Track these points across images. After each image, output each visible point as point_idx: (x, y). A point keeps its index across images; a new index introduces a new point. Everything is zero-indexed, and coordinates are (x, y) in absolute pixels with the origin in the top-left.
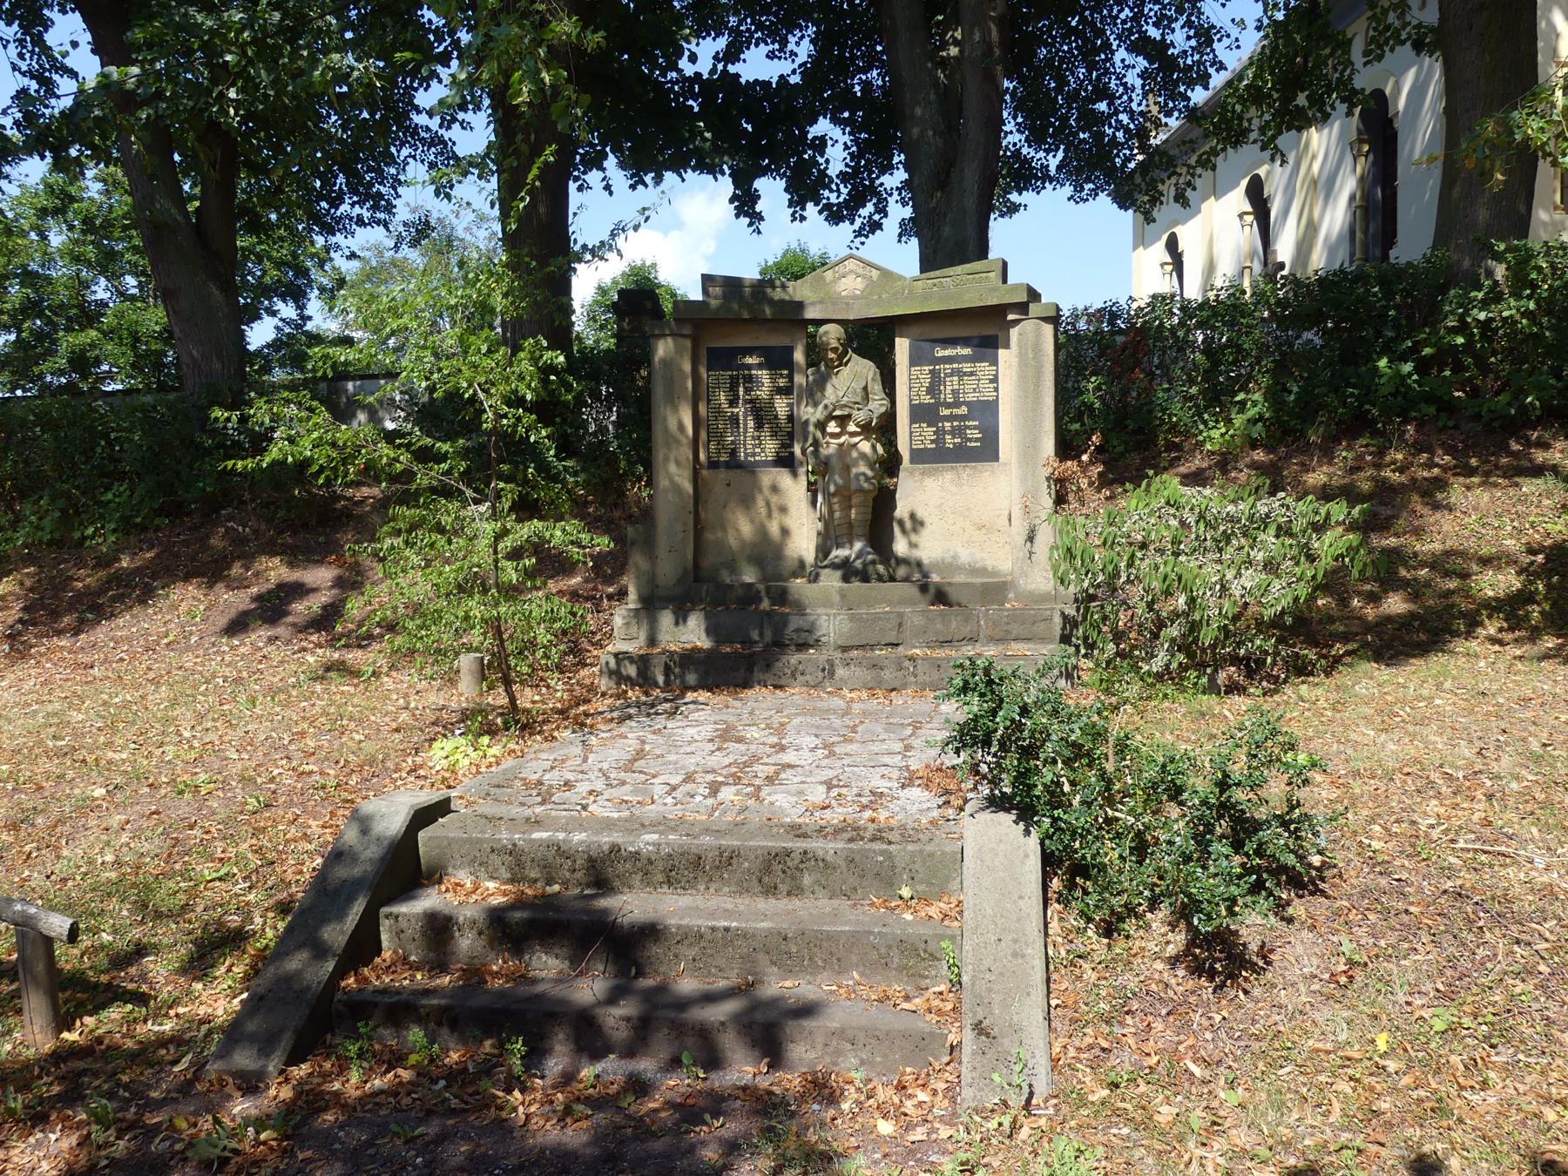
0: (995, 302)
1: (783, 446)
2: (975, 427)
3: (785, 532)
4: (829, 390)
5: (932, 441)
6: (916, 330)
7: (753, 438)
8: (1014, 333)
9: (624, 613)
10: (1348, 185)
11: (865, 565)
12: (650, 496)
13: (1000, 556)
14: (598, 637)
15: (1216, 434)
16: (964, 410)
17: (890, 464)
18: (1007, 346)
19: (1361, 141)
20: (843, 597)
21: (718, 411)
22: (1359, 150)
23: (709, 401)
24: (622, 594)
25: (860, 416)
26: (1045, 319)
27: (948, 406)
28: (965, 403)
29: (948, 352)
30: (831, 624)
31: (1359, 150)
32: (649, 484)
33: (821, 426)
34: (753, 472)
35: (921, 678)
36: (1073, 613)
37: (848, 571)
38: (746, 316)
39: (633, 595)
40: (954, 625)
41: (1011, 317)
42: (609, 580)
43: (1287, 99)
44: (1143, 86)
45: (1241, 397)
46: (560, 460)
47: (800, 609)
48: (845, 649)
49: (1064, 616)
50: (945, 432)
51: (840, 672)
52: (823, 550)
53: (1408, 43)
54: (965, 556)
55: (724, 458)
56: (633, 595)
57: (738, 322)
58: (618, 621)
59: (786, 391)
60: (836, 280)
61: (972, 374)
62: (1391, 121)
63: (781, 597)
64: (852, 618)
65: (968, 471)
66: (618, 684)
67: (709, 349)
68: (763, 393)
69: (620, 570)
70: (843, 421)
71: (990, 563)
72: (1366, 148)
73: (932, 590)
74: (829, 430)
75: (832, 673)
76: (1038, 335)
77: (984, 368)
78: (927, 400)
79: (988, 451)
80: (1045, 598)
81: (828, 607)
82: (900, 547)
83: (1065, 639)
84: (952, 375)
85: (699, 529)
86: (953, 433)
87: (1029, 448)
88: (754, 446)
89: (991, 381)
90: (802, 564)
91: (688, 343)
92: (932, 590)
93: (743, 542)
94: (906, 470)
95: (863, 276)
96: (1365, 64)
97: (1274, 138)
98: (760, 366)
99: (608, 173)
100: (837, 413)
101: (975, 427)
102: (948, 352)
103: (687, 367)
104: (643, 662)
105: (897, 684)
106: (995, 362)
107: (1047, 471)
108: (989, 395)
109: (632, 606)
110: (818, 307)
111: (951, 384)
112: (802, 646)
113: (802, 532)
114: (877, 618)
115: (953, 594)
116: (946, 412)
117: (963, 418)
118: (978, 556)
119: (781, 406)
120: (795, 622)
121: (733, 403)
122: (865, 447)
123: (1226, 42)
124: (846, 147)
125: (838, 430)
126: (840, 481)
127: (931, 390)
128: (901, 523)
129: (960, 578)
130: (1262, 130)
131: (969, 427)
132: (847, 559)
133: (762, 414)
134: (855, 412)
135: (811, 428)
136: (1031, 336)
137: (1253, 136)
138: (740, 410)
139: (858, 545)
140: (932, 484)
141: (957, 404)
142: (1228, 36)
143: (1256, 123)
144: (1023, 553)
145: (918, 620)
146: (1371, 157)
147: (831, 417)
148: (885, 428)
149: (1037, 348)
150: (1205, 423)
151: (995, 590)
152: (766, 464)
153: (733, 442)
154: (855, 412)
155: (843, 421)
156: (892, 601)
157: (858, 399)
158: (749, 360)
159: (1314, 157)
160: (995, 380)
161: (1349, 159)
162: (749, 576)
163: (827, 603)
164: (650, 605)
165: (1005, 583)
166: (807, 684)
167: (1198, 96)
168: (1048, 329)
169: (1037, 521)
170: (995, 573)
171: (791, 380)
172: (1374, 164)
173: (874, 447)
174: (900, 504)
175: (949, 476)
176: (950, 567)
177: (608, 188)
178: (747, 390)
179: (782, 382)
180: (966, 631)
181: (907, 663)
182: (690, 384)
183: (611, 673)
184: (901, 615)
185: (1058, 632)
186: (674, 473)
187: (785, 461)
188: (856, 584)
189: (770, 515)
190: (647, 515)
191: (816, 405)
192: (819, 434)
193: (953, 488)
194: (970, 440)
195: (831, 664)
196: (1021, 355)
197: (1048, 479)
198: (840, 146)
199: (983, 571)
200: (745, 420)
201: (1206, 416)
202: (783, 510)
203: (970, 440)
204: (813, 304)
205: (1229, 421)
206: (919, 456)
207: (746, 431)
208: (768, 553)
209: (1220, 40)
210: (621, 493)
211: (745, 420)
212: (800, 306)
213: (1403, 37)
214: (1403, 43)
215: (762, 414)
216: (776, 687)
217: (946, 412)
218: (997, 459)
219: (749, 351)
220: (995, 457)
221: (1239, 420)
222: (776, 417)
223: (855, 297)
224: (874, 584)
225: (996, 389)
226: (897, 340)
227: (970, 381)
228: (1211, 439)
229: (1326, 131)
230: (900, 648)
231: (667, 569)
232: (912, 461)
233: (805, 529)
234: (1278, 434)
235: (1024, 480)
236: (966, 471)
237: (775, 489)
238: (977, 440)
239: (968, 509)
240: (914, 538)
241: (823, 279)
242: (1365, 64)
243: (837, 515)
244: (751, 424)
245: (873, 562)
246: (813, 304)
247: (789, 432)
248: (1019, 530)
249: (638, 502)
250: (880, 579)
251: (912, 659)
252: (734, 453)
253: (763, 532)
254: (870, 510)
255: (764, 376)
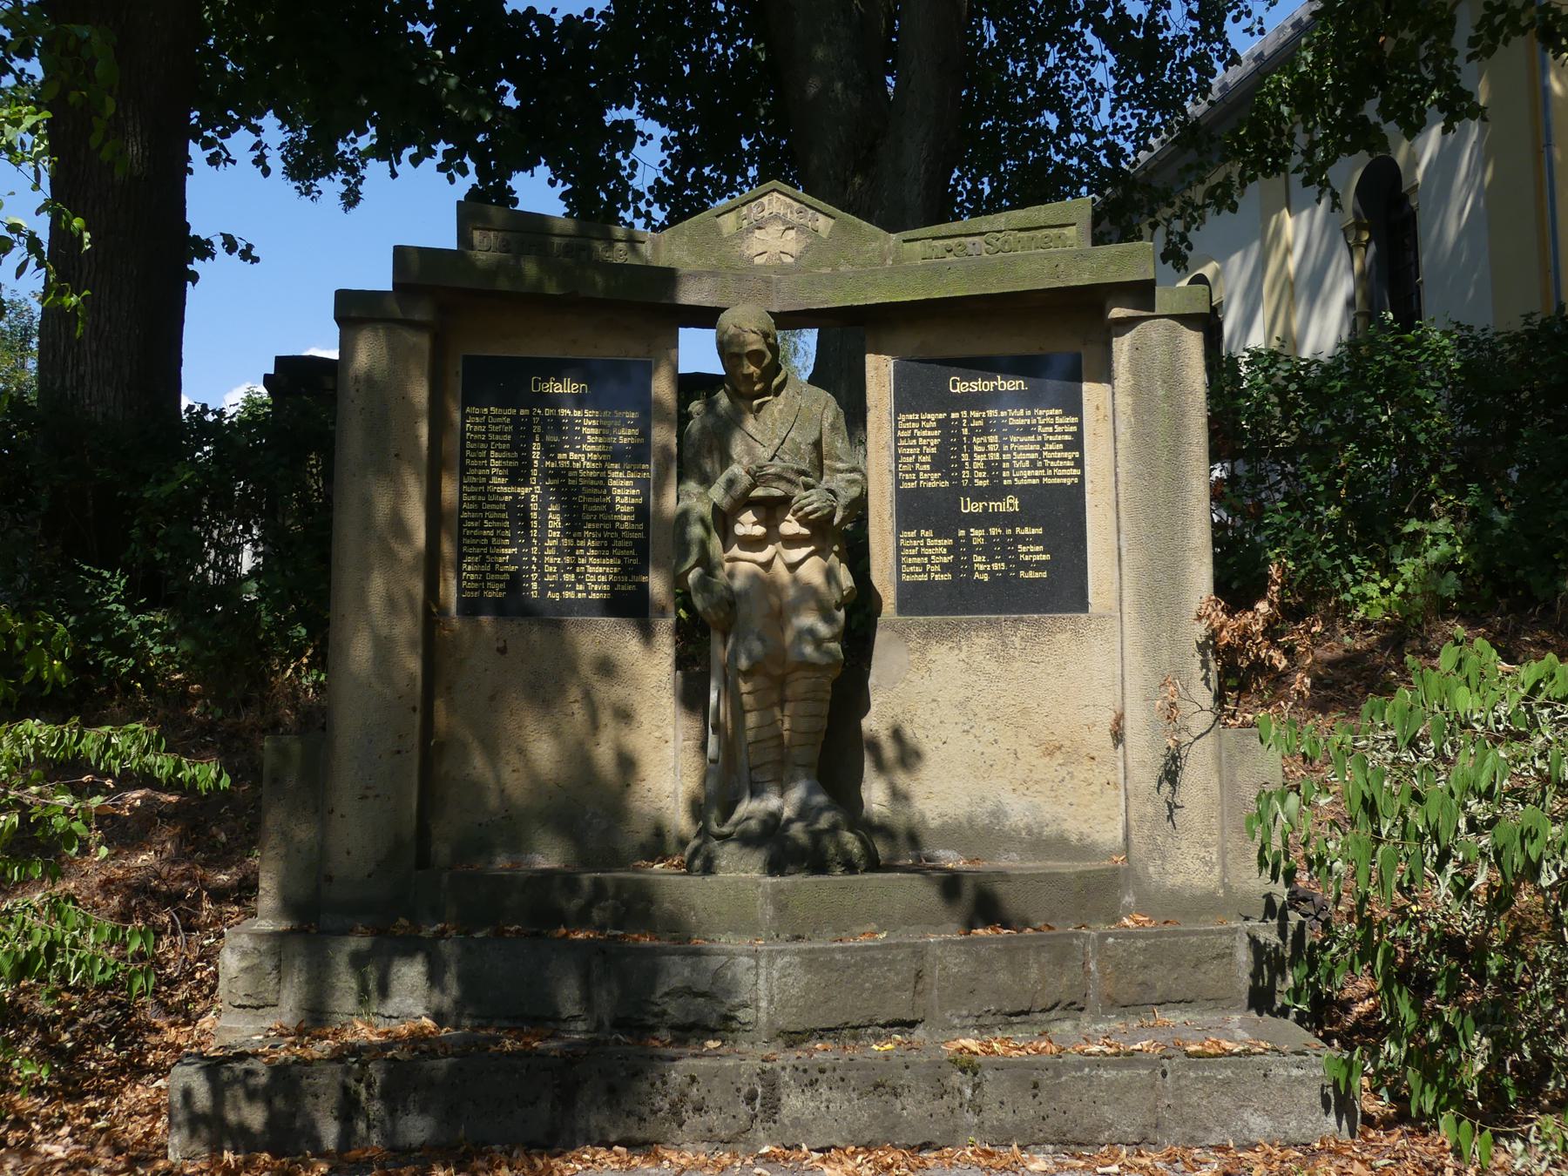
0: (1085, 279)
1: (625, 570)
2: (1036, 540)
3: (627, 764)
4: (737, 448)
5: (945, 568)
6: (911, 341)
7: (560, 551)
8: (1122, 347)
9: (246, 941)
10: (1342, 288)
11: (816, 836)
12: (317, 685)
13: (1094, 811)
14: (180, 996)
15: (1372, 590)
16: (1011, 504)
17: (859, 617)
18: (1105, 374)
19: (1358, 226)
20: (781, 907)
21: (484, 491)
22: (1357, 238)
23: (464, 470)
24: (245, 891)
25: (812, 500)
26: (1187, 320)
27: (979, 494)
28: (1012, 489)
29: (978, 386)
30: (765, 977)
31: (1357, 238)
32: (320, 661)
33: (723, 520)
34: (558, 625)
35: (993, 1115)
36: (1274, 939)
37: (780, 849)
38: (552, 288)
39: (267, 899)
40: (1034, 973)
41: (1117, 313)
42: (221, 859)
43: (1353, 106)
44: (1117, 89)
45: (1413, 525)
46: (134, 611)
47: (680, 933)
48: (793, 1038)
49: (1256, 945)
50: (971, 550)
51: (794, 1103)
52: (714, 801)
53: (1532, 32)
54: (1019, 811)
55: (494, 592)
56: (267, 899)
57: (533, 303)
58: (230, 962)
59: (637, 455)
60: (743, 233)
61: (1027, 430)
62: (1404, 198)
63: (638, 906)
64: (812, 961)
65: (1024, 631)
66: (216, 1150)
67: (468, 360)
68: (583, 457)
69: (249, 837)
70: (771, 510)
71: (1073, 827)
72: (1366, 236)
73: (968, 891)
74: (740, 530)
75: (772, 1107)
76: (1175, 351)
77: (1051, 418)
78: (934, 481)
79: (1064, 590)
80: (1206, 904)
81: (752, 936)
82: (875, 795)
83: (1261, 1000)
84: (985, 431)
85: (433, 752)
86: (988, 550)
87: (1160, 590)
88: (562, 569)
89: (1068, 446)
90: (659, 832)
91: (423, 342)
92: (968, 891)
93: (534, 777)
94: (891, 626)
95: (801, 229)
96: (1469, 58)
97: (1324, 166)
98: (579, 401)
99: (264, 137)
100: (759, 492)
101: (1036, 540)
102: (978, 386)
103: (420, 394)
104: (287, 1082)
105: (934, 1134)
106: (1074, 407)
107: (1200, 631)
108: (1067, 477)
109: (265, 925)
110: (708, 283)
111: (984, 450)
112: (691, 1031)
113: (668, 766)
114: (867, 958)
115: (1012, 899)
116: (974, 507)
117: (1009, 520)
118: (1048, 811)
119: (623, 491)
120: (678, 972)
121: (518, 475)
122: (812, 571)
123: (1245, 22)
124: (666, 145)
125: (759, 530)
126: (757, 647)
127: (941, 462)
128: (875, 747)
129: (1009, 861)
130: (1309, 154)
131: (1023, 540)
132: (774, 816)
133: (581, 503)
134: (799, 493)
135: (696, 531)
136: (1160, 353)
137: (1296, 160)
138: (533, 492)
139: (797, 794)
140: (945, 656)
141: (997, 491)
142: (1249, 14)
143: (1302, 140)
144: (1152, 808)
145: (956, 964)
146: (1372, 248)
147: (745, 502)
148: (844, 536)
149: (1173, 378)
150: (1352, 569)
151: (1099, 888)
152: (586, 607)
153: (514, 559)
154: (799, 493)
155: (771, 510)
156: (883, 917)
157: (804, 466)
158: (566, 387)
159: (1289, 250)
160: (1076, 443)
161: (1342, 253)
162: (548, 857)
163: (744, 924)
164: (311, 926)
165: (1115, 872)
166: (709, 1137)
167: (1194, 108)
168: (1193, 342)
169: (1185, 738)
170: (1085, 850)
171: (645, 433)
172: (1377, 257)
173: (830, 575)
174: (876, 699)
175: (982, 641)
176: (981, 834)
177: (260, 161)
178: (549, 451)
179: (625, 437)
180: (1060, 987)
181: (956, 1078)
182: (424, 431)
183: (195, 1122)
184: (919, 952)
185: (1244, 981)
186: (377, 624)
187: (628, 605)
188: (798, 881)
189: (594, 725)
190: (316, 722)
191: (706, 481)
192: (715, 543)
193: (991, 666)
194: (1027, 566)
195: (771, 1082)
196: (1137, 391)
197: (1202, 648)
198: (656, 144)
199: (1059, 846)
200: (543, 512)
201: (1355, 559)
202: (625, 715)
203: (1027, 566)
204: (697, 275)
205: (1388, 569)
206: (915, 598)
207: (542, 539)
208: (594, 803)
209: (1236, 19)
210: (261, 680)
211: (543, 512)
212: (669, 277)
213: (1523, 23)
214: (1524, 31)
215: (581, 503)
216: (631, 1145)
217: (974, 507)
218: (1082, 604)
219: (557, 369)
220: (1079, 602)
221: (1408, 568)
222: (610, 507)
223: (784, 270)
224: (838, 877)
225: (1079, 463)
226: (870, 359)
227: (1017, 439)
228: (1364, 598)
229: (1305, 214)
230: (919, 1033)
231: (355, 836)
232: (903, 607)
233: (669, 751)
234: (1486, 593)
235: (1151, 649)
236: (1019, 632)
237: (607, 668)
238: (1040, 566)
239: (1025, 711)
240: (902, 780)
241: (717, 229)
242: (1469, 58)
243: (751, 720)
244: (555, 521)
245: (834, 829)
246: (697, 275)
247: (639, 544)
248: (1143, 753)
249: (295, 693)
250: (850, 867)
251: (968, 1066)
252: (515, 583)
253: (581, 760)
254: (825, 709)
255: (587, 422)
